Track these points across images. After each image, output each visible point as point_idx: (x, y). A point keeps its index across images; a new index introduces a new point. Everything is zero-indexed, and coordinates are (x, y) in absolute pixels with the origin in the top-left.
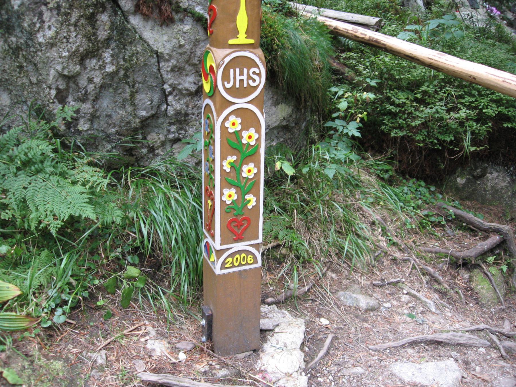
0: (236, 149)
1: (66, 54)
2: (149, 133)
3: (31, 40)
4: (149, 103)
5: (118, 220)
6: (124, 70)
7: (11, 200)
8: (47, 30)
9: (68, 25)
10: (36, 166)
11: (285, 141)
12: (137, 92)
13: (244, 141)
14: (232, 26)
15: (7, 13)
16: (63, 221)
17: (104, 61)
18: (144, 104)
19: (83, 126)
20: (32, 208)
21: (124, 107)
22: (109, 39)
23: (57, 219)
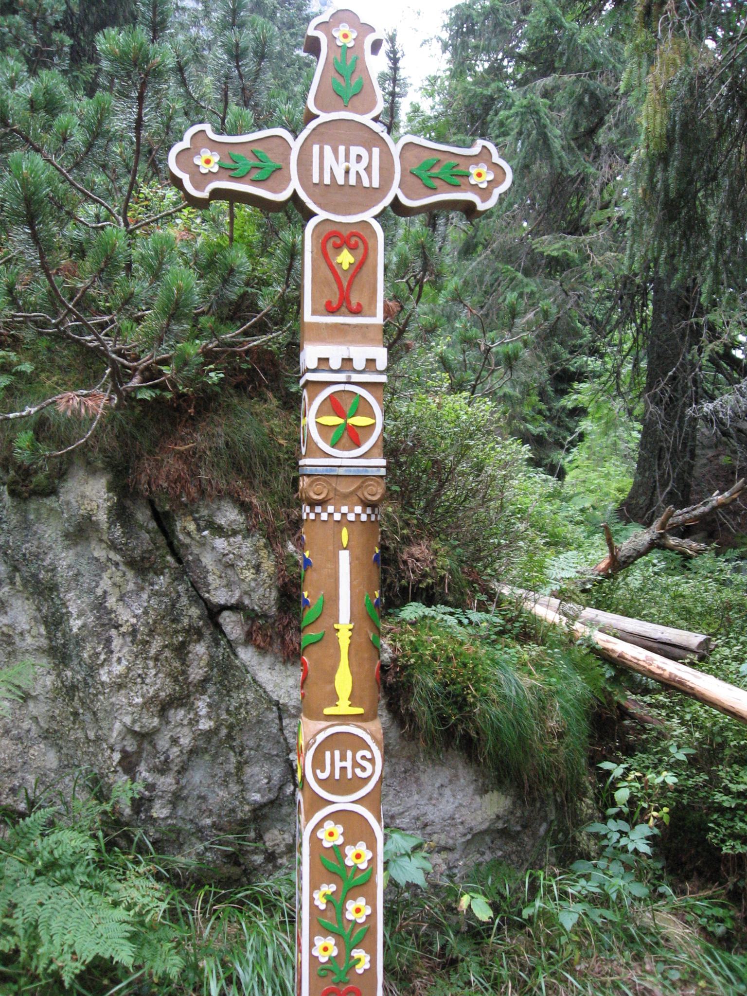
0: (334, 873)
1: (139, 700)
2: (268, 830)
3: (92, 676)
4: (266, 781)
5: (174, 973)
6: (227, 727)
7: (18, 923)
8: (115, 664)
9: (146, 658)
10: (63, 871)
11: (505, 856)
12: (246, 762)
13: (349, 862)
14: (328, 688)
15: (64, 635)
16: (83, 963)
17: (196, 714)
18: (258, 782)
19: (159, 811)
20: (45, 938)
21: (227, 786)
22: (206, 680)
23: (76, 960)
